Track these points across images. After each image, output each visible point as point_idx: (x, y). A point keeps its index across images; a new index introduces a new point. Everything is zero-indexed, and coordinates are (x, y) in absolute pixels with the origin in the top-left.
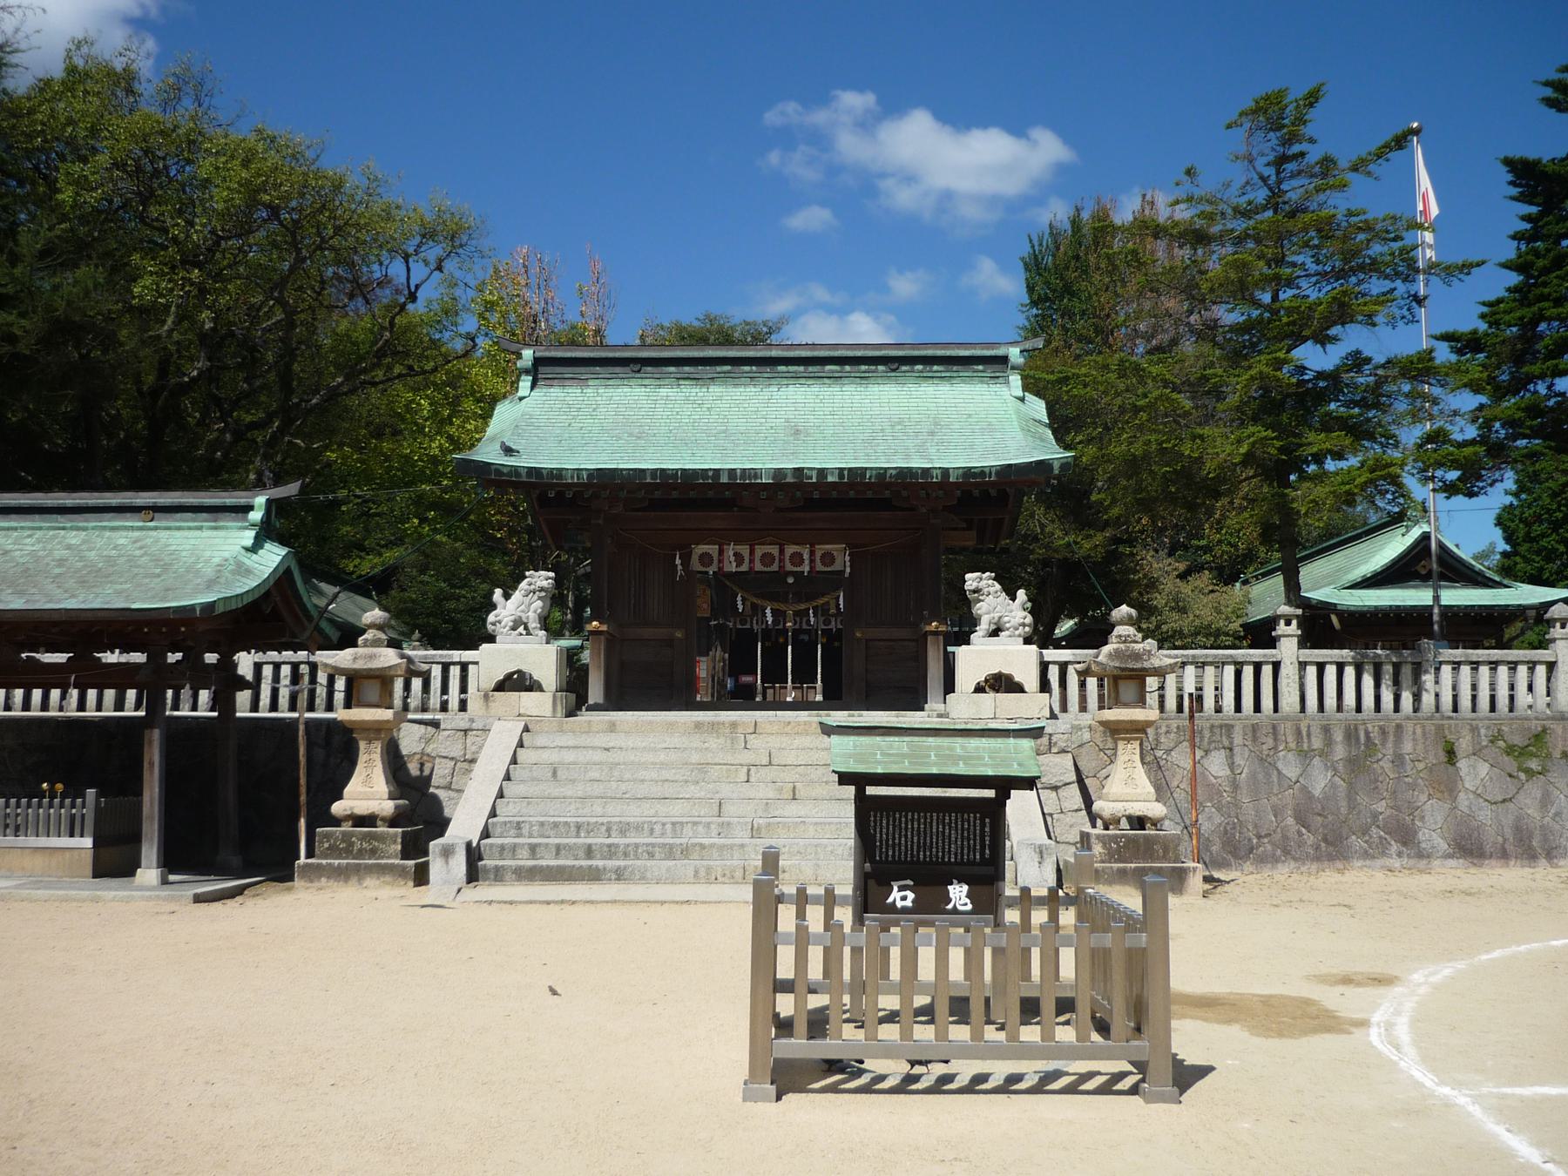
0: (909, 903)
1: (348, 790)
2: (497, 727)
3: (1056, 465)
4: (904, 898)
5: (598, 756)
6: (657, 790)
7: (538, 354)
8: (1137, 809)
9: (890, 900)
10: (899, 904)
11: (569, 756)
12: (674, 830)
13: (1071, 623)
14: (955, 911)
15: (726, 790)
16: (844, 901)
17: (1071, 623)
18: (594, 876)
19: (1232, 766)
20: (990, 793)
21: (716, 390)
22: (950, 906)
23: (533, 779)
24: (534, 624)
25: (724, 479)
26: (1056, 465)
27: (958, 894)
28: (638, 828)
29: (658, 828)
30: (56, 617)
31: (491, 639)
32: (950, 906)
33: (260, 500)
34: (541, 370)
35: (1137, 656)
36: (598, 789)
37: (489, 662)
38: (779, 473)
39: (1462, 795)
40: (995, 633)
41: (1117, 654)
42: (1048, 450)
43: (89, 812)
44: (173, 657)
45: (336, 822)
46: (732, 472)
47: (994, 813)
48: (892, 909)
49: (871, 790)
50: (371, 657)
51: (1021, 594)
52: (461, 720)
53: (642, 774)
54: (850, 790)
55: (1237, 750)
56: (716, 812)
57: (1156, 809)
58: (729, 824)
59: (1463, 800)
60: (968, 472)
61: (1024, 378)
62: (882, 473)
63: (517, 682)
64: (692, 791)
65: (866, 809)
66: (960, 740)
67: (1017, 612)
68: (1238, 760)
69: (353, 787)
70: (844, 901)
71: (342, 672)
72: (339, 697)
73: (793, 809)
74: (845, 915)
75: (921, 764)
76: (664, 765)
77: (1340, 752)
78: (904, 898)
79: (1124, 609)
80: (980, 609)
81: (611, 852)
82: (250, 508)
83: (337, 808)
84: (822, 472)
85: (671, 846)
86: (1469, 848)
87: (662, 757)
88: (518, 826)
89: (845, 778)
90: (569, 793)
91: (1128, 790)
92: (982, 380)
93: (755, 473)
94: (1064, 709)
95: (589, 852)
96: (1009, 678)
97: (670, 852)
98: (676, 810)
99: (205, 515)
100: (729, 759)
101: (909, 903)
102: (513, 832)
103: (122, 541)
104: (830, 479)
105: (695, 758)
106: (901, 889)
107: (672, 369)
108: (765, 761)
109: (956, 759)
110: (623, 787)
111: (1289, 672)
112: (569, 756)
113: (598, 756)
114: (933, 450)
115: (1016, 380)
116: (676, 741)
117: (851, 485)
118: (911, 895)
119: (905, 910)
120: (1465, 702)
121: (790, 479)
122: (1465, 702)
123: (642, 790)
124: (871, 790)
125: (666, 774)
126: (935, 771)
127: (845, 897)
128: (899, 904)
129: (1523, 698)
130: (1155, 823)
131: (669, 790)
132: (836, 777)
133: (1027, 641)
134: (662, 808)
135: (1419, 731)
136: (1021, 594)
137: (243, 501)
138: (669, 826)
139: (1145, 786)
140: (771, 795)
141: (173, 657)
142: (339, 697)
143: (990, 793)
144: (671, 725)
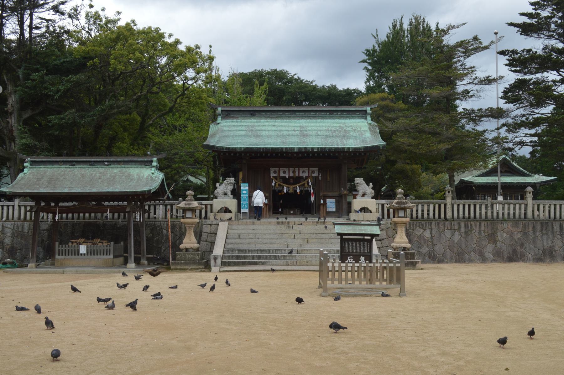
1: (184, 241)
3: (381, 147)
5: (251, 231)
6: (269, 241)
7: (223, 109)
8: (403, 245)
13: (165, 59)
15: (289, 241)
17: (165, 59)
18: (255, 264)
19: (431, 234)
20: (369, 238)
21: (278, 121)
24: (229, 193)
25: (284, 151)
26: (381, 147)
28: (266, 251)
30: (108, 194)
31: (216, 198)
33: (155, 159)
34: (227, 115)
35: (404, 203)
36: (252, 241)
37: (217, 204)
38: (300, 149)
39: (498, 243)
40: (364, 195)
41: (397, 203)
42: (380, 142)
43: (112, 248)
44: (280, 210)
45: (181, 250)
46: (286, 148)
47: (370, 241)
49: (344, 237)
50: (189, 204)
51: (371, 184)
54: (339, 237)
55: (433, 229)
57: (408, 245)
59: (499, 244)
60: (355, 149)
61: (371, 117)
62: (330, 149)
63: (227, 211)
64: (279, 241)
65: (343, 241)
67: (369, 189)
68: (433, 232)
69: (185, 240)
71: (181, 208)
72: (391, 216)
73: (307, 246)
76: (270, 234)
77: (463, 230)
79: (400, 190)
80: (359, 188)
81: (259, 257)
82: (152, 161)
83: (181, 246)
84: (313, 149)
85: (276, 256)
87: (269, 232)
88: (232, 251)
89: (338, 234)
91: (400, 240)
92: (359, 118)
93: (293, 149)
94: (383, 217)
95: (253, 257)
96: (367, 209)
97: (275, 257)
98: (275, 247)
99: (134, 163)
100: (288, 232)
102: (231, 252)
103: (115, 171)
104: (315, 151)
105: (279, 232)
107: (264, 114)
108: (299, 232)
109: (362, 230)
111: (449, 207)
112: (243, 232)
114: (345, 141)
115: (369, 118)
117: (321, 152)
120: (425, 215)
121: (303, 151)
122: (425, 215)
123: (265, 241)
124: (344, 237)
126: (358, 232)
129: (536, 213)
130: (409, 249)
133: (372, 198)
134: (272, 246)
136: (371, 184)
137: (150, 159)
139: (406, 239)
140: (301, 242)
141: (280, 210)
142: (391, 216)
143: (369, 238)
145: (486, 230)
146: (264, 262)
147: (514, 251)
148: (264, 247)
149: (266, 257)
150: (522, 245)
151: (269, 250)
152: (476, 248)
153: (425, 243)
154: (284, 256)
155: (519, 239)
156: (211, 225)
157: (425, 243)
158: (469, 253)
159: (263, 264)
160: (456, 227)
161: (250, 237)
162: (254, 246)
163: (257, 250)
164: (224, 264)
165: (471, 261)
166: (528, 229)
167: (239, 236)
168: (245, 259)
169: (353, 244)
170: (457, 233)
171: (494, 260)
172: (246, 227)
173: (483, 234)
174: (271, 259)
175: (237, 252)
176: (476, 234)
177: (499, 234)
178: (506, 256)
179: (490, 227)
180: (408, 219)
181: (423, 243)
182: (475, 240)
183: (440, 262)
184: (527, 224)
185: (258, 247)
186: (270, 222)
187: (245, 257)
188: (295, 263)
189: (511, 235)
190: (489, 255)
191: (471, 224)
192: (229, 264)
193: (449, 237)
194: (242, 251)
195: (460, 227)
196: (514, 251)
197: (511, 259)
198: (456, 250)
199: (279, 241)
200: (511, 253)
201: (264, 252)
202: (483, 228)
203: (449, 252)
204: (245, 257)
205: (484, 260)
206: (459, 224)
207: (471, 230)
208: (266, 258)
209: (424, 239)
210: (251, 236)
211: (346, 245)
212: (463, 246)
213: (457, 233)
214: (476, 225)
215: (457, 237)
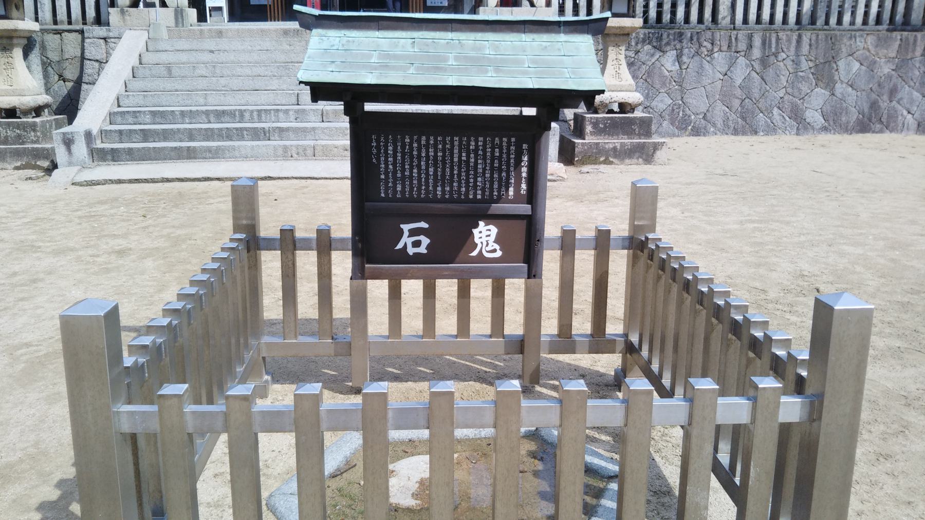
0: (422, 250)
2: (128, 35)
4: (417, 244)
5: (206, 57)
6: (250, 84)
9: (400, 246)
10: (411, 251)
11: (184, 57)
12: (259, 116)
14: (481, 258)
16: (341, 244)
22: (474, 253)
23: (153, 76)
27: (485, 236)
28: (231, 114)
29: (247, 115)
32: (474, 253)
36: (202, 83)
39: (838, 85)
48: (403, 257)
49: (369, 107)
52: (100, 31)
53: (239, 71)
56: (294, 101)
57: (634, 97)
58: (304, 110)
59: (839, 88)
64: (275, 84)
65: (368, 137)
66: (491, 36)
70: (341, 244)
74: (342, 263)
75: (437, 69)
77: (757, 53)
78: (417, 244)
86: (835, 121)
90: (180, 87)
97: (258, 135)
98: (262, 100)
101: (422, 250)
102: (131, 120)
105: (283, 58)
106: (413, 233)
109: (479, 63)
110: (223, 81)
113: (206, 57)
116: (267, 44)
118: (425, 241)
119: (418, 259)
123: (235, 83)
125: (261, 70)
127: (342, 240)
128: (411, 251)
131: (259, 84)
132: (306, 92)
134: (252, 98)
135: (814, 38)
138: (255, 114)
144: (249, 31)
145: (813, 53)
146: (218, 148)
147: (874, 105)
148: (231, 103)
149: (228, 135)
150: (893, 92)
151: (242, 113)
152: (786, 97)
153: (664, 84)
154: (281, 130)
155: (889, 77)
156: (105, 39)
157: (664, 84)
158: (768, 112)
159: (215, 155)
160: (742, 46)
161: (199, 72)
162: (202, 101)
163: (207, 113)
164: (100, 156)
165: (771, 130)
166: (914, 51)
167: (169, 70)
168: (165, 139)
169: (427, 147)
170: (742, 61)
171: (825, 129)
172: (195, 45)
173: (805, 65)
174: (242, 138)
175: (148, 118)
176: (789, 63)
177: (841, 64)
178: (854, 116)
179: (822, 45)
180: (638, 22)
181: (658, 86)
182: (783, 80)
183: (697, 132)
184: (911, 40)
185: (215, 102)
186: (262, 31)
187: (166, 135)
188: (310, 152)
189: (871, 66)
190: (814, 116)
191: (778, 39)
192: (113, 156)
193: (724, 70)
194: (162, 114)
195: (750, 47)
196: (874, 105)
197: (863, 127)
198: (736, 103)
199: (275, 84)
200: (866, 110)
201: (227, 118)
202: (805, 48)
203: (720, 109)
204: (166, 135)
205: (802, 125)
206: (750, 37)
207: (776, 55)
208: (229, 138)
209: (662, 76)
210: (202, 71)
211: (388, 157)
212: (756, 94)
213: (742, 61)
214: (789, 40)
215: (741, 71)
